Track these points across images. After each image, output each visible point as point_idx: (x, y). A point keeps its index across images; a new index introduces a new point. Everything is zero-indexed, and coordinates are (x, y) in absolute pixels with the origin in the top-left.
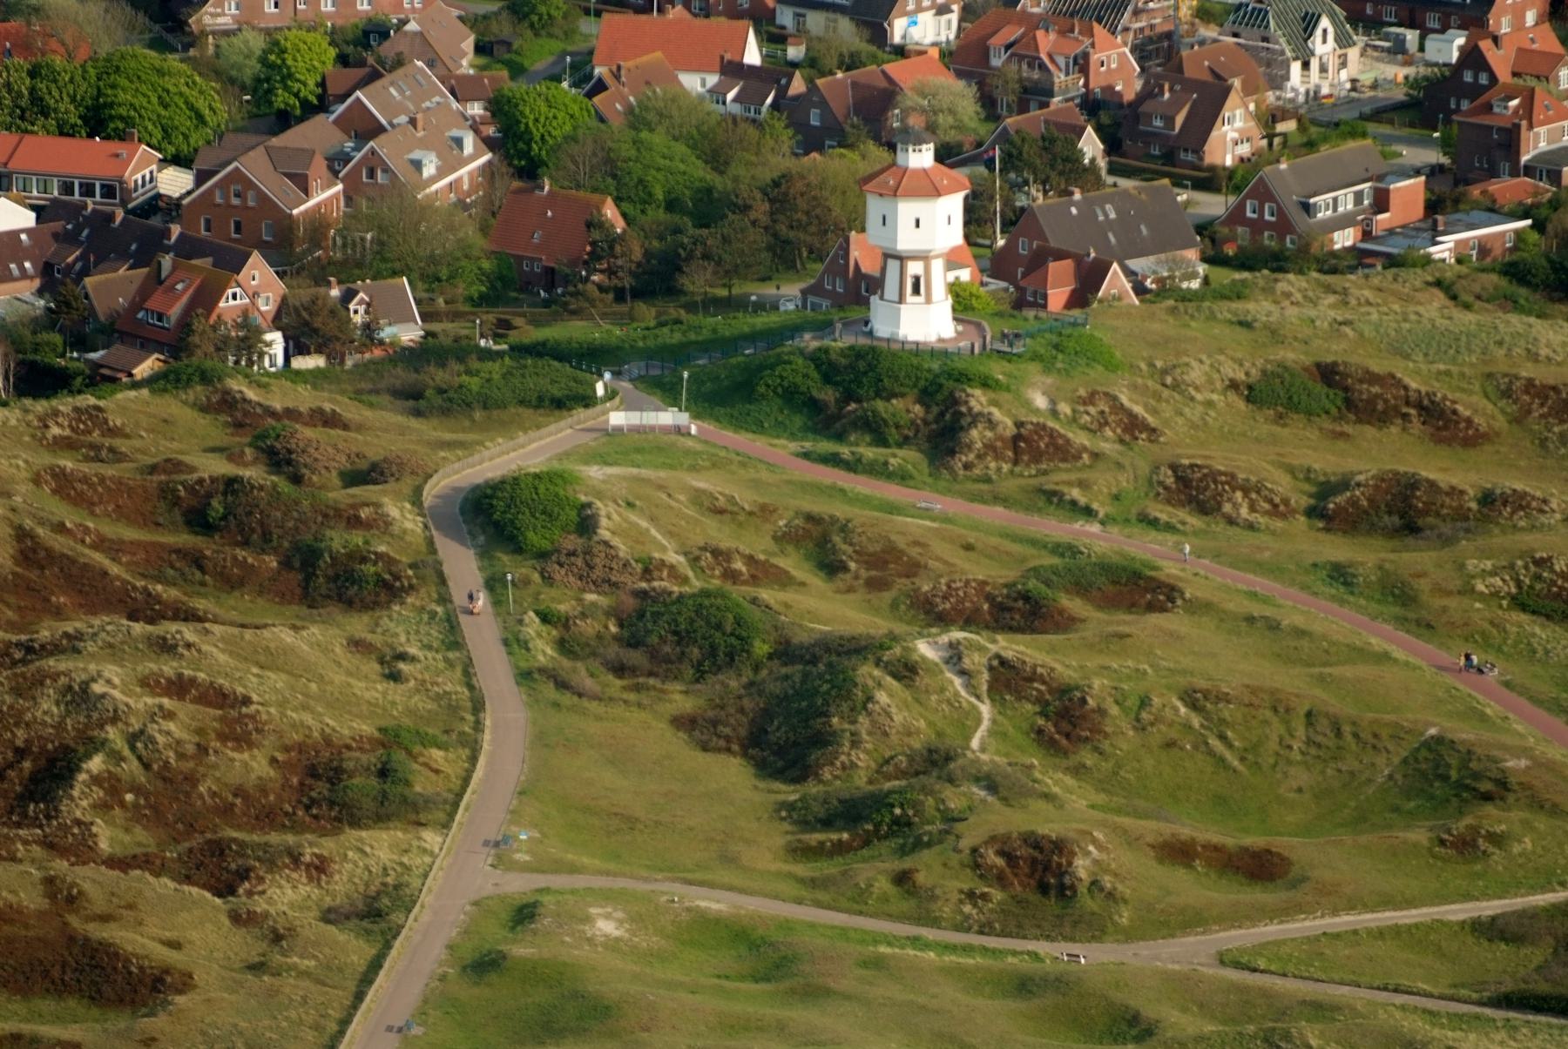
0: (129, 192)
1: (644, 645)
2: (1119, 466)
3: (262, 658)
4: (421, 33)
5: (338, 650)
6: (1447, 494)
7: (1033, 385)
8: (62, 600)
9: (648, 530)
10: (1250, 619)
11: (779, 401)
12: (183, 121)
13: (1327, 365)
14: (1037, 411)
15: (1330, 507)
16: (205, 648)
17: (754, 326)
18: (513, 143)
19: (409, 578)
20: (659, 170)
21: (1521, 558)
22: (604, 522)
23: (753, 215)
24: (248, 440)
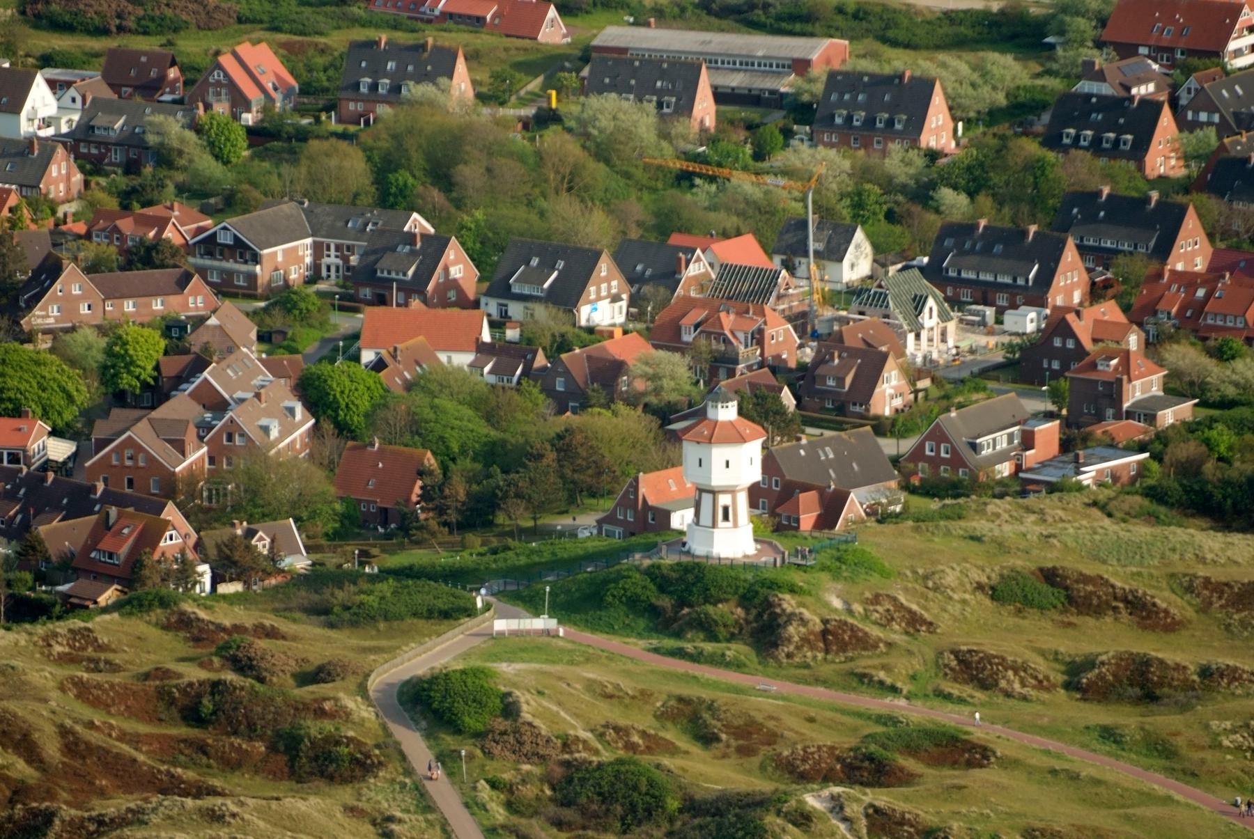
0: (30, 458)
1: (575, 804)
2: (910, 653)
3: (288, 824)
4: (220, 327)
5: (339, 815)
6: (1174, 669)
7: (828, 590)
8: (104, 782)
10: (1054, 772)
11: (625, 608)
12: (58, 400)
14: (836, 610)
15: (1079, 679)
16: (247, 816)
17: (586, 549)
19: (376, 756)
20: (452, 428)
22: (525, 707)
24: (213, 650)
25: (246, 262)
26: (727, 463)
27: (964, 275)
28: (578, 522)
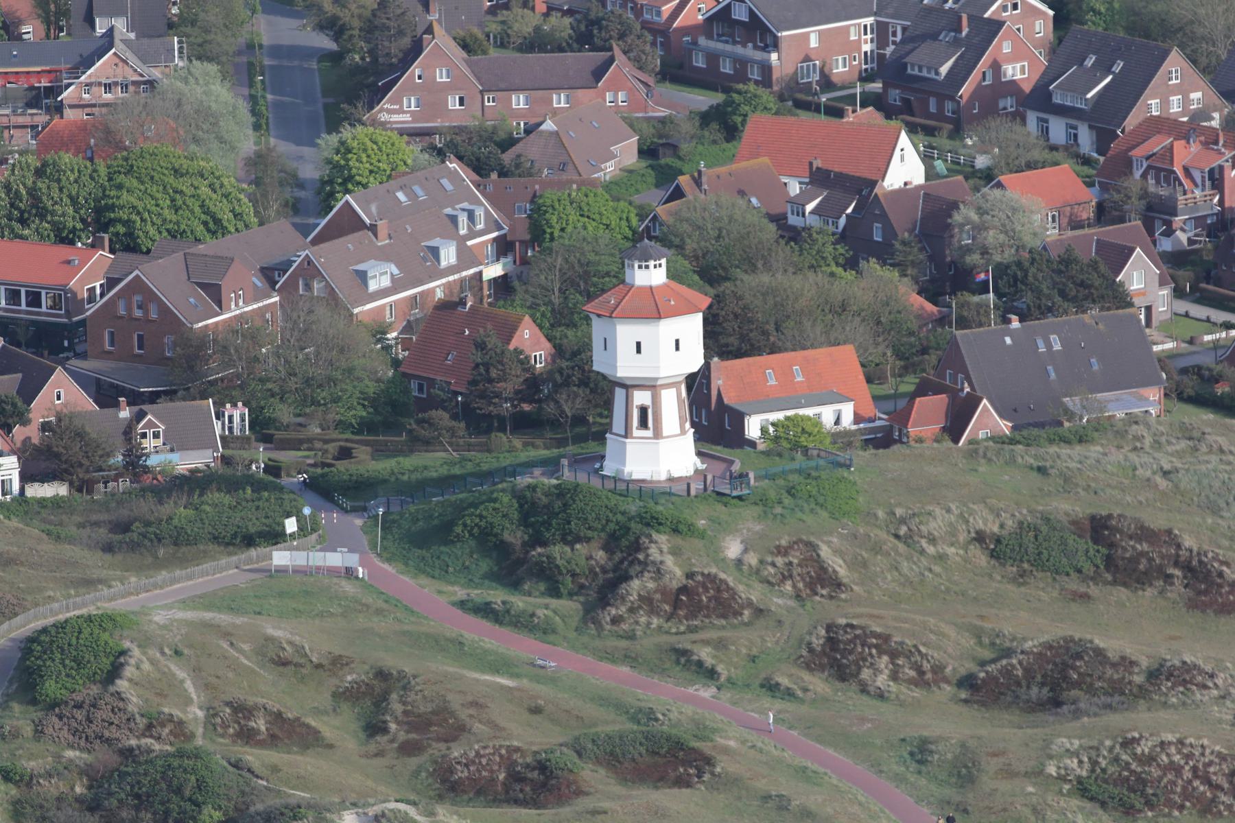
4: (557, 133)
6: (1114, 665)
9: (182, 682)
11: (472, 543)
13: (1102, 517)
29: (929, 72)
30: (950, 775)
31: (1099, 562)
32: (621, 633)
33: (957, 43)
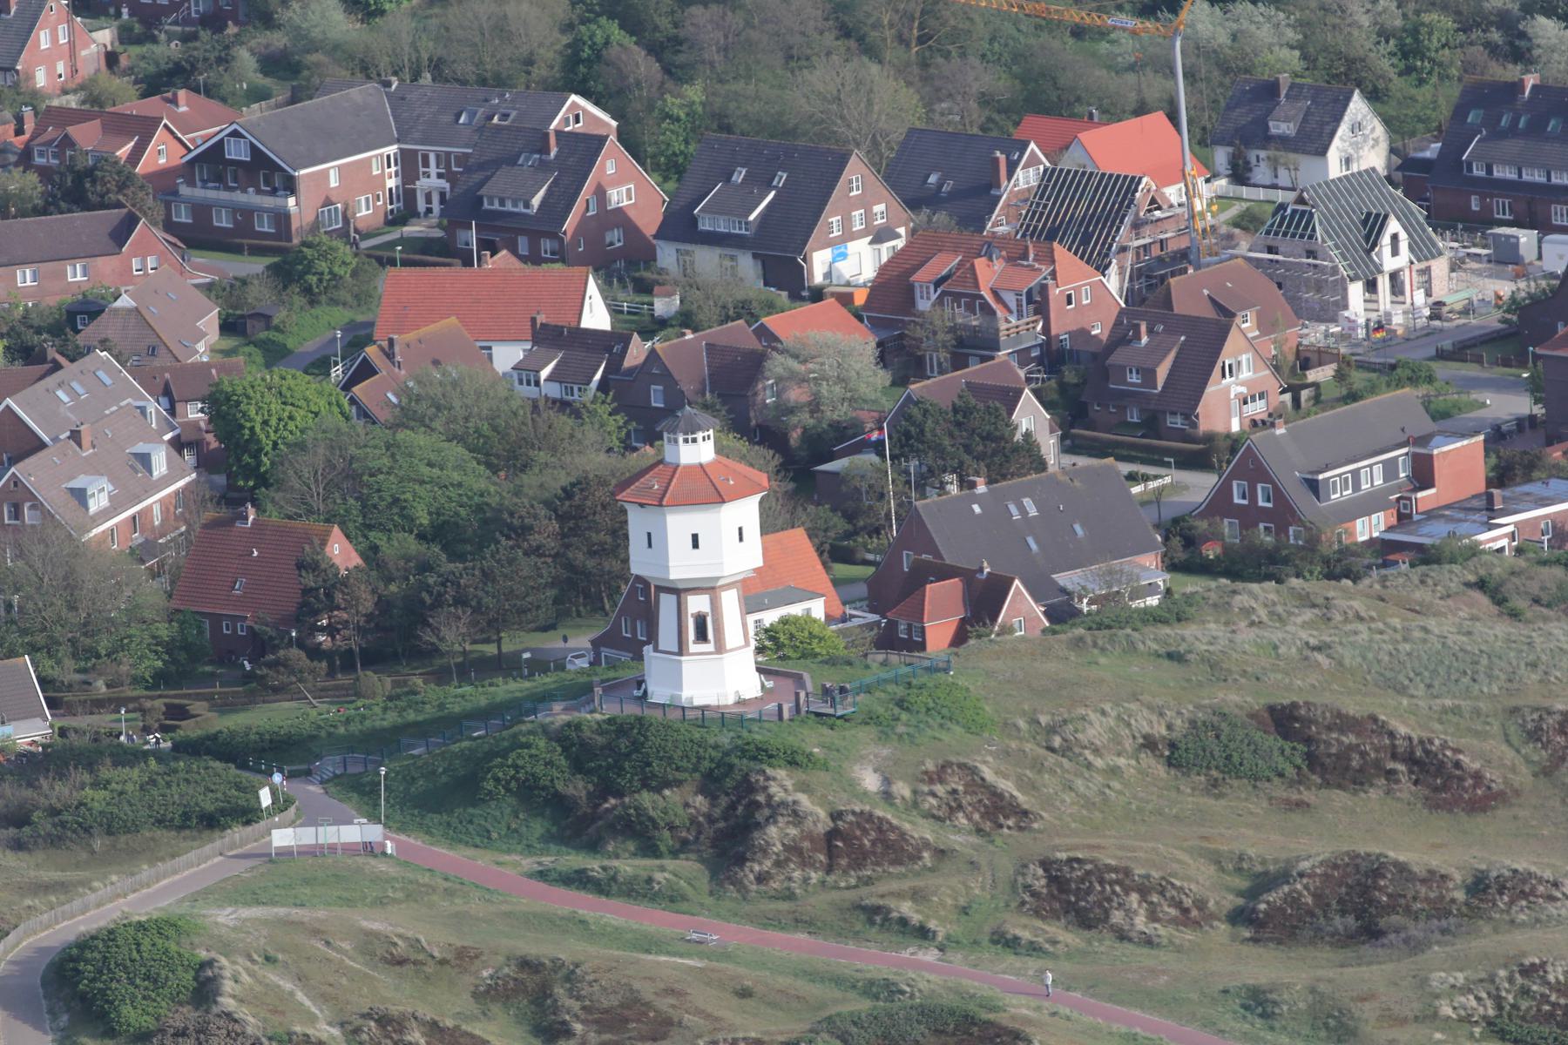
6: (1423, 881)
9: (292, 994)
11: (512, 800)
13: (1284, 707)
15: (1267, 911)
18: (232, 460)
20: (422, 482)
21: (1505, 966)
22: (228, 986)
23: (535, 539)
25: (274, 192)
26: (696, 545)
27: (1498, 173)
28: (571, 644)
29: (515, 205)
30: (1313, 1028)
31: (1299, 761)
32: (773, 893)
33: (544, 166)
